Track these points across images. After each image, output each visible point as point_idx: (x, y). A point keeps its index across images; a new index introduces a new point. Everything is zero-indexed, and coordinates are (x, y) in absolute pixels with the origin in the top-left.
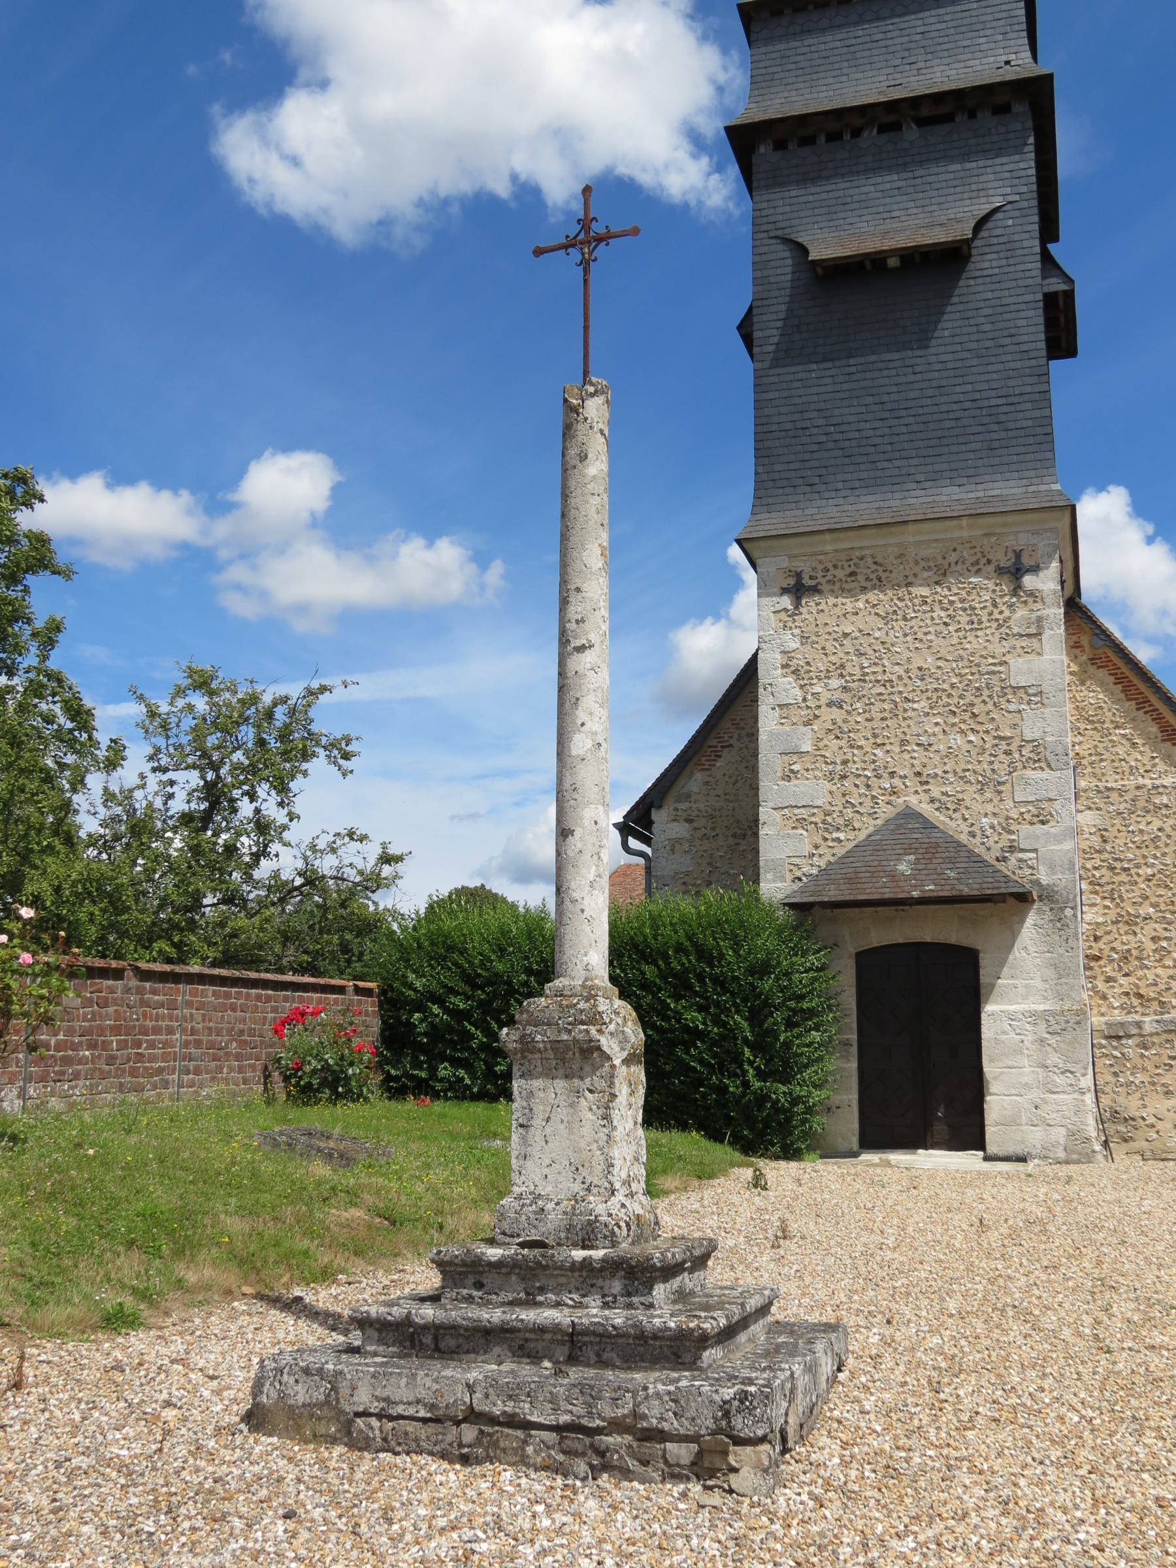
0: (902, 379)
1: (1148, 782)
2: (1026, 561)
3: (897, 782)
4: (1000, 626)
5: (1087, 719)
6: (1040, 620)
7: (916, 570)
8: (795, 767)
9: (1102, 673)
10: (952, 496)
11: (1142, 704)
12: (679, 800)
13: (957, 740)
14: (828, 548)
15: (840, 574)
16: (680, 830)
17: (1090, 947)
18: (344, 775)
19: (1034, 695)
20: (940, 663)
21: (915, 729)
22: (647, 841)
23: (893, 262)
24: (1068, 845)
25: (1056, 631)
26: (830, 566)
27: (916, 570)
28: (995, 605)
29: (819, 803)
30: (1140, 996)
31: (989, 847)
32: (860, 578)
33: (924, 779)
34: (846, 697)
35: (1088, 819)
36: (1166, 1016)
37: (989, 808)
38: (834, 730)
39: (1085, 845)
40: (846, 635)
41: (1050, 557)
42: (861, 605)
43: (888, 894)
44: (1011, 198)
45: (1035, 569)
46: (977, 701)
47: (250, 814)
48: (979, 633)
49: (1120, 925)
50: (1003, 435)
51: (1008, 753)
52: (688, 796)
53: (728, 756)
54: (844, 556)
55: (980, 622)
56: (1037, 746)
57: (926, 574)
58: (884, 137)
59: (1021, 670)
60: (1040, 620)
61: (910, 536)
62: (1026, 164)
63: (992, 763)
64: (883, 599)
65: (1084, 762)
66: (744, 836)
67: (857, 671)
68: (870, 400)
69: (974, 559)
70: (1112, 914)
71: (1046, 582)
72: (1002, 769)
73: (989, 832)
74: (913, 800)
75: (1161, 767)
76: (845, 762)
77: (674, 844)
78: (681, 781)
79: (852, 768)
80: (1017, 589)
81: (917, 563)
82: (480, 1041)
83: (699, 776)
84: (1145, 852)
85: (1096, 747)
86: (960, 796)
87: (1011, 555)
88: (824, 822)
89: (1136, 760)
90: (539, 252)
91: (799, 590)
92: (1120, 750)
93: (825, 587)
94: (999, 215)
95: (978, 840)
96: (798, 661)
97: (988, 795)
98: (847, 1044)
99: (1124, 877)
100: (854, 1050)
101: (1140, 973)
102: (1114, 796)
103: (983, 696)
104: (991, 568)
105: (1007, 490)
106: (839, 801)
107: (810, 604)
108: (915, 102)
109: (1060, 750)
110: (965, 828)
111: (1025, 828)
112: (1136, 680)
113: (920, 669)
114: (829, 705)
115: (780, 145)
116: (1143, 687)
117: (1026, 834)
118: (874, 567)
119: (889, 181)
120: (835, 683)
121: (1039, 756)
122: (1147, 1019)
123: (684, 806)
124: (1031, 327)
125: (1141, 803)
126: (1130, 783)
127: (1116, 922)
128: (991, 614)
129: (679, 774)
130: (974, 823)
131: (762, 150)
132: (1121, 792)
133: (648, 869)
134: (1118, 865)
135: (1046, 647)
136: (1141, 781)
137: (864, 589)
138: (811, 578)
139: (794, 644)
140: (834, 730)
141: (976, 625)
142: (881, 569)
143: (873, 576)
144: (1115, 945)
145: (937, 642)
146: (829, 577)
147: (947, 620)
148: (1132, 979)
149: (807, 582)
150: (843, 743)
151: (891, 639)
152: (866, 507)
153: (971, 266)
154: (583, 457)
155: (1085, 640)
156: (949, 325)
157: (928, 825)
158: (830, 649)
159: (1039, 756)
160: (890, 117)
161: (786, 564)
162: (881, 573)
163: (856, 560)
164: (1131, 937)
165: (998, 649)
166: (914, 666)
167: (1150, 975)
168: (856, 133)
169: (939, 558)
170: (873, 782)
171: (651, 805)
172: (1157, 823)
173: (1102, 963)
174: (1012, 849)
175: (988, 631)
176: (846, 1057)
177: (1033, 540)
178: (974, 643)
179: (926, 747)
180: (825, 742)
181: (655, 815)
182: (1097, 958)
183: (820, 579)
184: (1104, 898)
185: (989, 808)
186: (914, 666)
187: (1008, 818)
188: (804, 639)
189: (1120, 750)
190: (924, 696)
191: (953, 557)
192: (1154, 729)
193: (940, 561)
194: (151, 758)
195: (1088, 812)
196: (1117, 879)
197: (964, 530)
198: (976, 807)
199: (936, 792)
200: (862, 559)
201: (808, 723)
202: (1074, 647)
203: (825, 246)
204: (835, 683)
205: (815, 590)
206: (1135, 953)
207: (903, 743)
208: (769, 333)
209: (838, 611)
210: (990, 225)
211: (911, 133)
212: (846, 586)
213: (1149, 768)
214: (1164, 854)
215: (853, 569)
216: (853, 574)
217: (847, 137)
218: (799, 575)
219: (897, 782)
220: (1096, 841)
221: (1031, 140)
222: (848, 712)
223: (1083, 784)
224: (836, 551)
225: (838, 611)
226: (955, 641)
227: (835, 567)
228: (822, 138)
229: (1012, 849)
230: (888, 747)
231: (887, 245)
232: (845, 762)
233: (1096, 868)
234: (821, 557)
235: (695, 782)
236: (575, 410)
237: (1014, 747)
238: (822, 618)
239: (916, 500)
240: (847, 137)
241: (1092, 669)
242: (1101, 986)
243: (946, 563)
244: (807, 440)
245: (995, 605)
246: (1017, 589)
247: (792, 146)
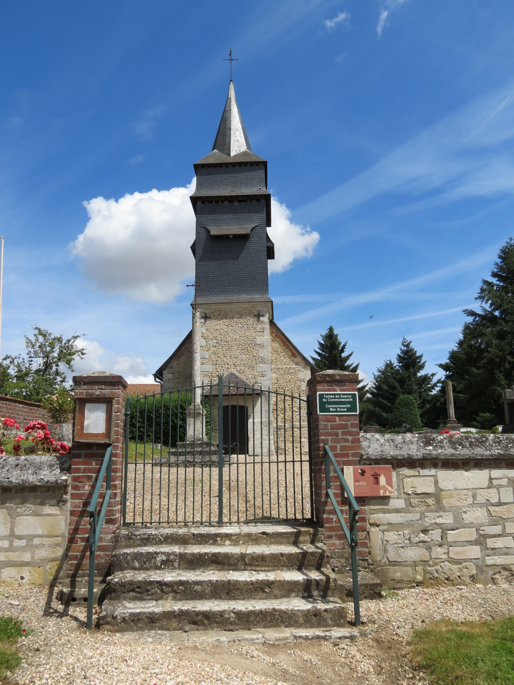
0: (232, 266)
1: (288, 367)
2: (261, 314)
3: (229, 366)
5: (274, 350)
6: (264, 328)
7: (235, 314)
9: (278, 339)
10: (244, 297)
11: (287, 347)
12: (170, 368)
13: (243, 356)
14: (213, 307)
15: (216, 314)
16: (170, 376)
18: (82, 359)
19: (262, 346)
21: (234, 353)
22: (161, 380)
23: (231, 237)
24: (269, 382)
25: (267, 326)
31: (250, 382)
35: (274, 375)
37: (251, 373)
38: (214, 353)
39: (273, 382)
40: (217, 329)
41: (267, 313)
42: (221, 322)
45: (263, 316)
47: (55, 370)
50: (256, 282)
51: (255, 360)
52: (173, 367)
53: (183, 357)
54: (217, 310)
56: (262, 358)
58: (230, 204)
59: (259, 340)
60: (264, 328)
61: (234, 306)
62: (264, 215)
64: (227, 321)
66: (187, 378)
67: (220, 338)
68: (224, 271)
71: (265, 319)
72: (254, 364)
74: (233, 370)
75: (292, 363)
76: (216, 361)
77: (169, 380)
78: (171, 363)
79: (218, 362)
80: (259, 320)
82: (498, 285)
83: (176, 362)
90: (187, 286)
91: (206, 317)
92: (282, 358)
93: (212, 317)
94: (257, 227)
95: (248, 380)
97: (251, 370)
98: (216, 429)
100: (218, 431)
102: (280, 370)
103: (251, 346)
104: (253, 315)
105: (257, 297)
106: (215, 370)
107: (208, 322)
108: (237, 196)
109: (267, 359)
110: (245, 378)
111: (259, 378)
112: (286, 341)
115: (203, 202)
116: (288, 343)
117: (259, 379)
119: (230, 216)
120: (215, 341)
121: (263, 361)
123: (172, 370)
124: (265, 253)
125: (287, 372)
126: (284, 367)
129: (170, 362)
130: (248, 377)
131: (199, 203)
132: (282, 369)
133: (162, 386)
135: (265, 335)
136: (287, 366)
137: (222, 319)
139: (204, 331)
140: (214, 353)
141: (249, 329)
145: (240, 332)
149: (208, 316)
151: (228, 331)
152: (223, 298)
153: (250, 240)
154: (196, 322)
155: (274, 331)
156: (244, 253)
157: (237, 377)
158: (213, 333)
159: (263, 361)
160: (231, 199)
165: (254, 335)
166: (233, 338)
168: (223, 202)
170: (223, 366)
171: (163, 369)
172: (290, 377)
174: (256, 383)
176: (216, 433)
177: (263, 308)
178: (248, 333)
179: (236, 358)
181: (164, 372)
185: (251, 373)
186: (233, 338)
188: (207, 330)
189: (282, 358)
191: (244, 312)
192: (290, 354)
194: (28, 354)
197: (247, 306)
198: (248, 373)
199: (238, 369)
201: (207, 351)
202: (272, 332)
203: (215, 231)
204: (215, 341)
205: (210, 318)
207: (231, 357)
208: (199, 251)
209: (216, 323)
210: (255, 230)
211: (236, 204)
216: (219, 314)
217: (220, 202)
218: (206, 314)
219: (229, 366)
220: (276, 381)
221: (265, 209)
223: (273, 366)
225: (216, 323)
228: (214, 202)
229: (256, 383)
231: (230, 232)
232: (216, 361)
235: (174, 364)
236: (195, 314)
237: (257, 359)
238: (211, 325)
239: (235, 298)
240: (220, 202)
241: (276, 338)
244: (208, 280)
246: (259, 320)
247: (206, 203)
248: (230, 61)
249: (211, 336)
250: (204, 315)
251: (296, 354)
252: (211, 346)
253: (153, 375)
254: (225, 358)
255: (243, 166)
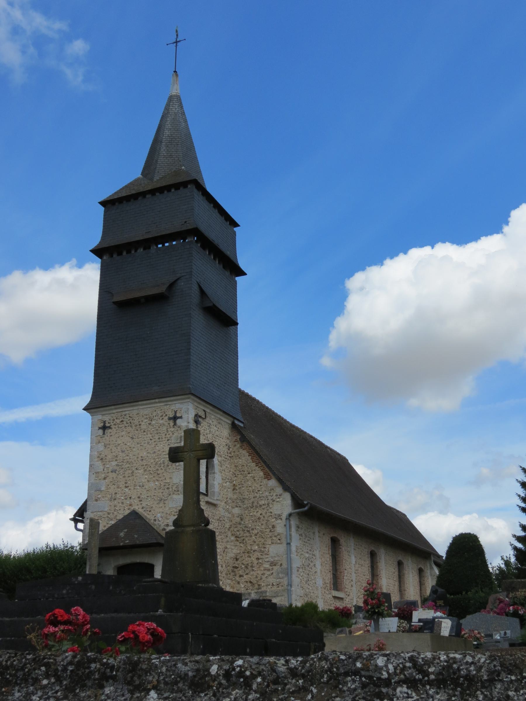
4: (168, 440)
7: (143, 419)
8: (99, 496)
17: (234, 563)
20: (149, 455)
26: (115, 418)
27: (143, 419)
28: (167, 431)
29: (106, 510)
30: (251, 582)
32: (125, 423)
33: (141, 499)
34: (118, 468)
36: (260, 590)
37: (161, 510)
43: (113, 544)
44: (183, 275)
46: (160, 469)
48: (161, 443)
49: (246, 554)
55: (162, 438)
57: (146, 420)
63: (162, 493)
65: (237, 488)
69: (161, 414)
70: (243, 549)
73: (160, 519)
79: (118, 496)
81: (143, 416)
84: (255, 523)
85: (241, 481)
86: (152, 506)
87: (173, 412)
88: (108, 517)
89: (255, 486)
93: (113, 427)
96: (103, 456)
99: (248, 534)
101: (252, 573)
113: (142, 457)
114: (112, 472)
118: (129, 418)
120: (114, 463)
122: (253, 592)
125: (255, 504)
127: (244, 553)
128: (166, 435)
134: (246, 529)
138: (109, 423)
142: (131, 419)
143: (128, 422)
144: (243, 562)
146: (115, 423)
147: (151, 438)
148: (249, 576)
150: (115, 486)
161: (101, 418)
162: (131, 421)
163: (123, 416)
164: (249, 558)
166: (140, 456)
167: (255, 573)
169: (150, 414)
172: (260, 512)
173: (238, 569)
175: (164, 442)
180: (109, 486)
182: (237, 568)
183: (112, 424)
184: (240, 543)
185: (161, 510)
186: (140, 456)
187: (167, 514)
190: (142, 467)
191: (154, 414)
193: (151, 415)
195: (236, 508)
196: (245, 535)
200: (125, 415)
206: (250, 565)
212: (119, 426)
213: (259, 489)
214: (262, 524)
215: (122, 419)
216: (122, 421)
220: (238, 520)
222: (118, 474)
224: (117, 412)
226: (153, 446)
227: (117, 418)
230: (129, 488)
233: (238, 531)
234: (112, 415)
242: (237, 578)
243: (152, 416)
245: (167, 431)
248: (175, 44)
249: (109, 457)
250: (102, 424)
251: (270, 474)
252: (110, 471)
253: (71, 519)
254: (127, 490)
255: (166, 192)
